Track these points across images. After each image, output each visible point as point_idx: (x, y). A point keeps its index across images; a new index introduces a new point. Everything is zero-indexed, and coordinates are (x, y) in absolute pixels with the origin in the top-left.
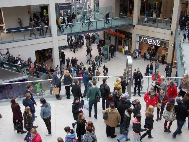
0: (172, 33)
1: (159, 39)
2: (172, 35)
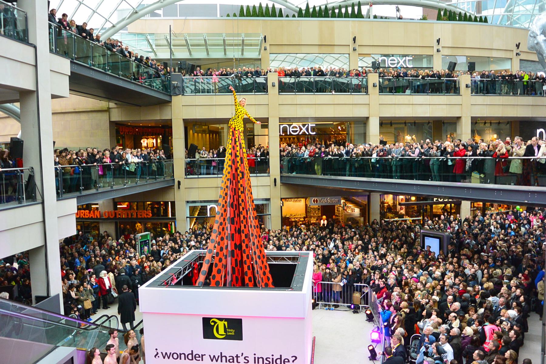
0: (275, 180)
2: (275, 185)
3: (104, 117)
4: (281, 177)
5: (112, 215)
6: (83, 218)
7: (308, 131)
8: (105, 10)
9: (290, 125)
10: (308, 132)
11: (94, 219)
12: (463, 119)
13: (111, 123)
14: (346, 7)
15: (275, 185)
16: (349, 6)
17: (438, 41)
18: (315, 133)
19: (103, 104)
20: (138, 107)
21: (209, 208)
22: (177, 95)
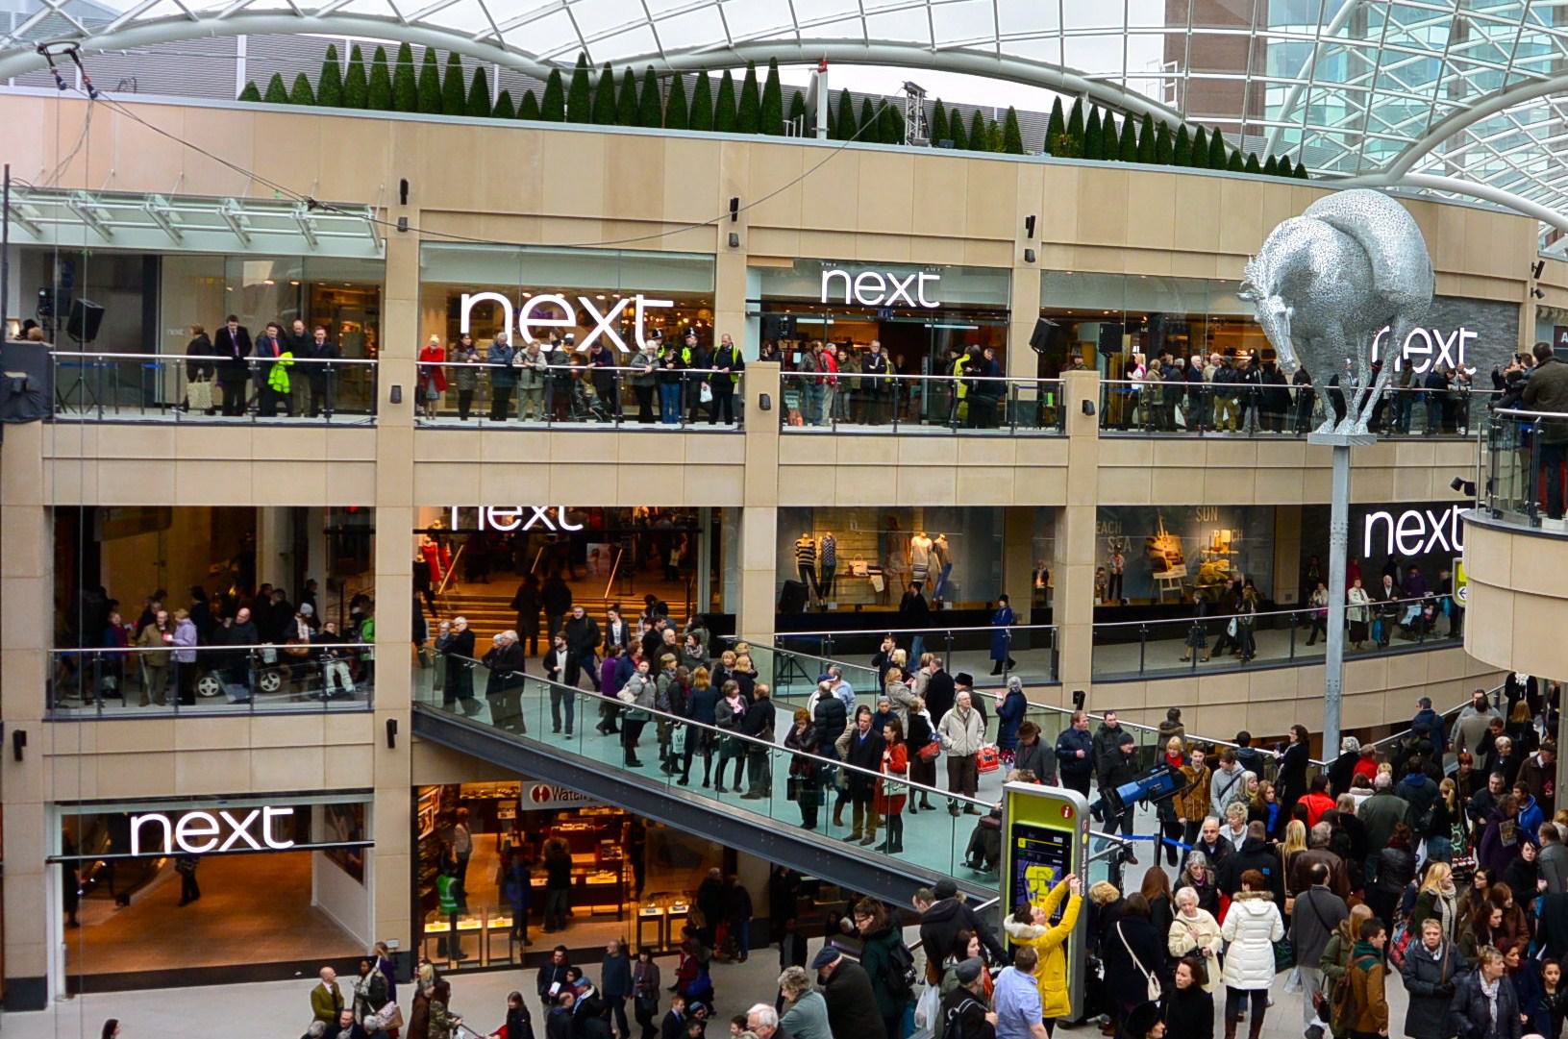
0: (392, 726)
1: (936, 517)
2: (391, 744)
9: (174, 818)
14: (751, 65)
15: (391, 744)
16: (762, 63)
18: (579, 527)
21: (136, 824)
22: (24, 420)
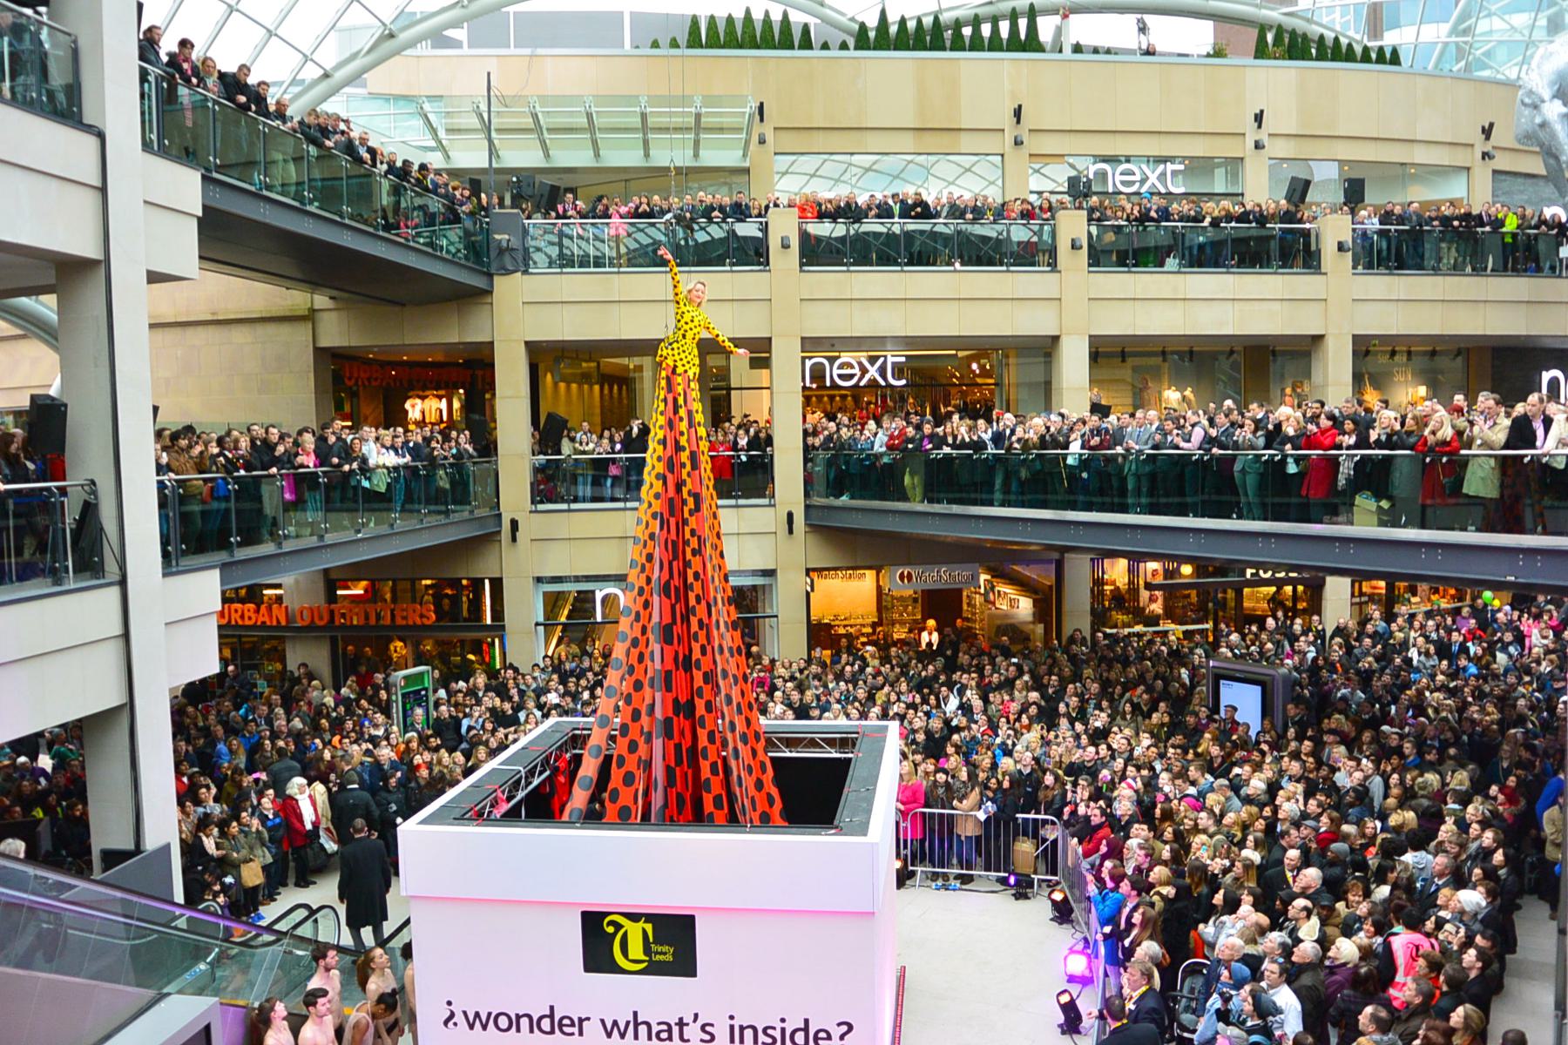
0: (790, 516)
2: (791, 531)
3: (299, 337)
4: (807, 507)
5: (321, 619)
6: (237, 626)
7: (884, 377)
8: (301, 30)
9: (832, 360)
10: (885, 378)
11: (271, 628)
12: (1330, 343)
13: (320, 353)
14: (995, 20)
15: (791, 531)
16: (1004, 17)
17: (1259, 118)
18: (903, 382)
19: (296, 299)
20: (397, 309)
21: (599, 596)
